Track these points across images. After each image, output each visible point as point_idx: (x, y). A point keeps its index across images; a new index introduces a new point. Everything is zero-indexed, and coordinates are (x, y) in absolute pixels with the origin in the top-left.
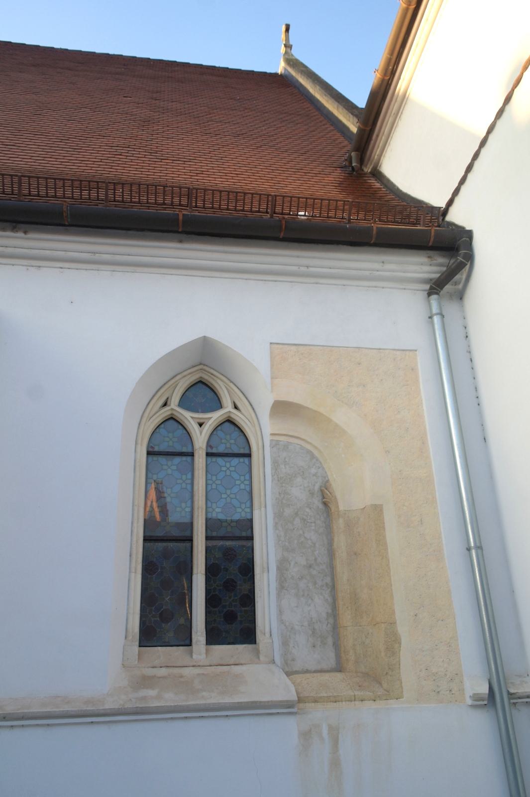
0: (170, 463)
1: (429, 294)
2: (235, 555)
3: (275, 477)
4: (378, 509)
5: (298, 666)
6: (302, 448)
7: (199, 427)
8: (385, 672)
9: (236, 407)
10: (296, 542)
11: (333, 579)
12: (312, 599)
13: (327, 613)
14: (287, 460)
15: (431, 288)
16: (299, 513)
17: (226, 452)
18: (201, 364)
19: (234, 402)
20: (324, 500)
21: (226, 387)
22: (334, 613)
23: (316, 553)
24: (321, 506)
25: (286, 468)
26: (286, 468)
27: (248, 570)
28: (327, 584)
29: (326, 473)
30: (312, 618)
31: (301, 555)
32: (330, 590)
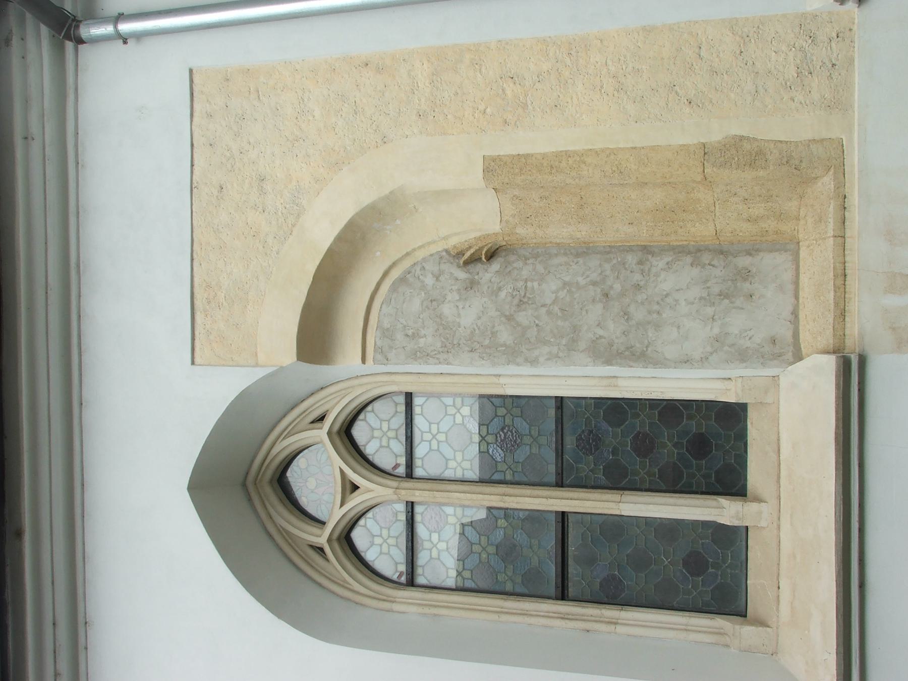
0: (427, 545)
1: (80, 41)
2: (591, 432)
3: (442, 357)
4: (493, 167)
5: (784, 332)
6: (387, 301)
7: (357, 492)
8: (794, 171)
9: (321, 419)
10: (560, 323)
11: (630, 249)
12: (667, 295)
13: (692, 265)
14: (410, 333)
15: (68, 37)
16: (508, 313)
17: (403, 439)
18: (244, 485)
19: (312, 422)
20: (483, 259)
21: (284, 438)
22: (694, 252)
23: (581, 281)
24: (496, 266)
25: (425, 336)
26: (425, 336)
27: (617, 409)
28: (640, 263)
29: (431, 255)
30: (701, 298)
31: (584, 313)
32: (650, 257)
